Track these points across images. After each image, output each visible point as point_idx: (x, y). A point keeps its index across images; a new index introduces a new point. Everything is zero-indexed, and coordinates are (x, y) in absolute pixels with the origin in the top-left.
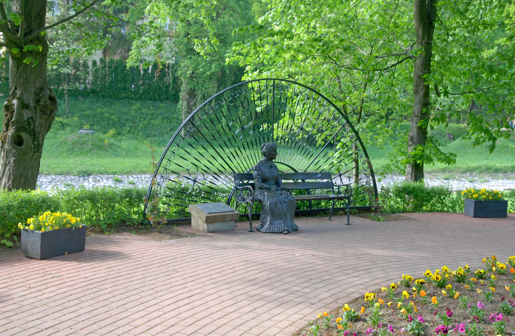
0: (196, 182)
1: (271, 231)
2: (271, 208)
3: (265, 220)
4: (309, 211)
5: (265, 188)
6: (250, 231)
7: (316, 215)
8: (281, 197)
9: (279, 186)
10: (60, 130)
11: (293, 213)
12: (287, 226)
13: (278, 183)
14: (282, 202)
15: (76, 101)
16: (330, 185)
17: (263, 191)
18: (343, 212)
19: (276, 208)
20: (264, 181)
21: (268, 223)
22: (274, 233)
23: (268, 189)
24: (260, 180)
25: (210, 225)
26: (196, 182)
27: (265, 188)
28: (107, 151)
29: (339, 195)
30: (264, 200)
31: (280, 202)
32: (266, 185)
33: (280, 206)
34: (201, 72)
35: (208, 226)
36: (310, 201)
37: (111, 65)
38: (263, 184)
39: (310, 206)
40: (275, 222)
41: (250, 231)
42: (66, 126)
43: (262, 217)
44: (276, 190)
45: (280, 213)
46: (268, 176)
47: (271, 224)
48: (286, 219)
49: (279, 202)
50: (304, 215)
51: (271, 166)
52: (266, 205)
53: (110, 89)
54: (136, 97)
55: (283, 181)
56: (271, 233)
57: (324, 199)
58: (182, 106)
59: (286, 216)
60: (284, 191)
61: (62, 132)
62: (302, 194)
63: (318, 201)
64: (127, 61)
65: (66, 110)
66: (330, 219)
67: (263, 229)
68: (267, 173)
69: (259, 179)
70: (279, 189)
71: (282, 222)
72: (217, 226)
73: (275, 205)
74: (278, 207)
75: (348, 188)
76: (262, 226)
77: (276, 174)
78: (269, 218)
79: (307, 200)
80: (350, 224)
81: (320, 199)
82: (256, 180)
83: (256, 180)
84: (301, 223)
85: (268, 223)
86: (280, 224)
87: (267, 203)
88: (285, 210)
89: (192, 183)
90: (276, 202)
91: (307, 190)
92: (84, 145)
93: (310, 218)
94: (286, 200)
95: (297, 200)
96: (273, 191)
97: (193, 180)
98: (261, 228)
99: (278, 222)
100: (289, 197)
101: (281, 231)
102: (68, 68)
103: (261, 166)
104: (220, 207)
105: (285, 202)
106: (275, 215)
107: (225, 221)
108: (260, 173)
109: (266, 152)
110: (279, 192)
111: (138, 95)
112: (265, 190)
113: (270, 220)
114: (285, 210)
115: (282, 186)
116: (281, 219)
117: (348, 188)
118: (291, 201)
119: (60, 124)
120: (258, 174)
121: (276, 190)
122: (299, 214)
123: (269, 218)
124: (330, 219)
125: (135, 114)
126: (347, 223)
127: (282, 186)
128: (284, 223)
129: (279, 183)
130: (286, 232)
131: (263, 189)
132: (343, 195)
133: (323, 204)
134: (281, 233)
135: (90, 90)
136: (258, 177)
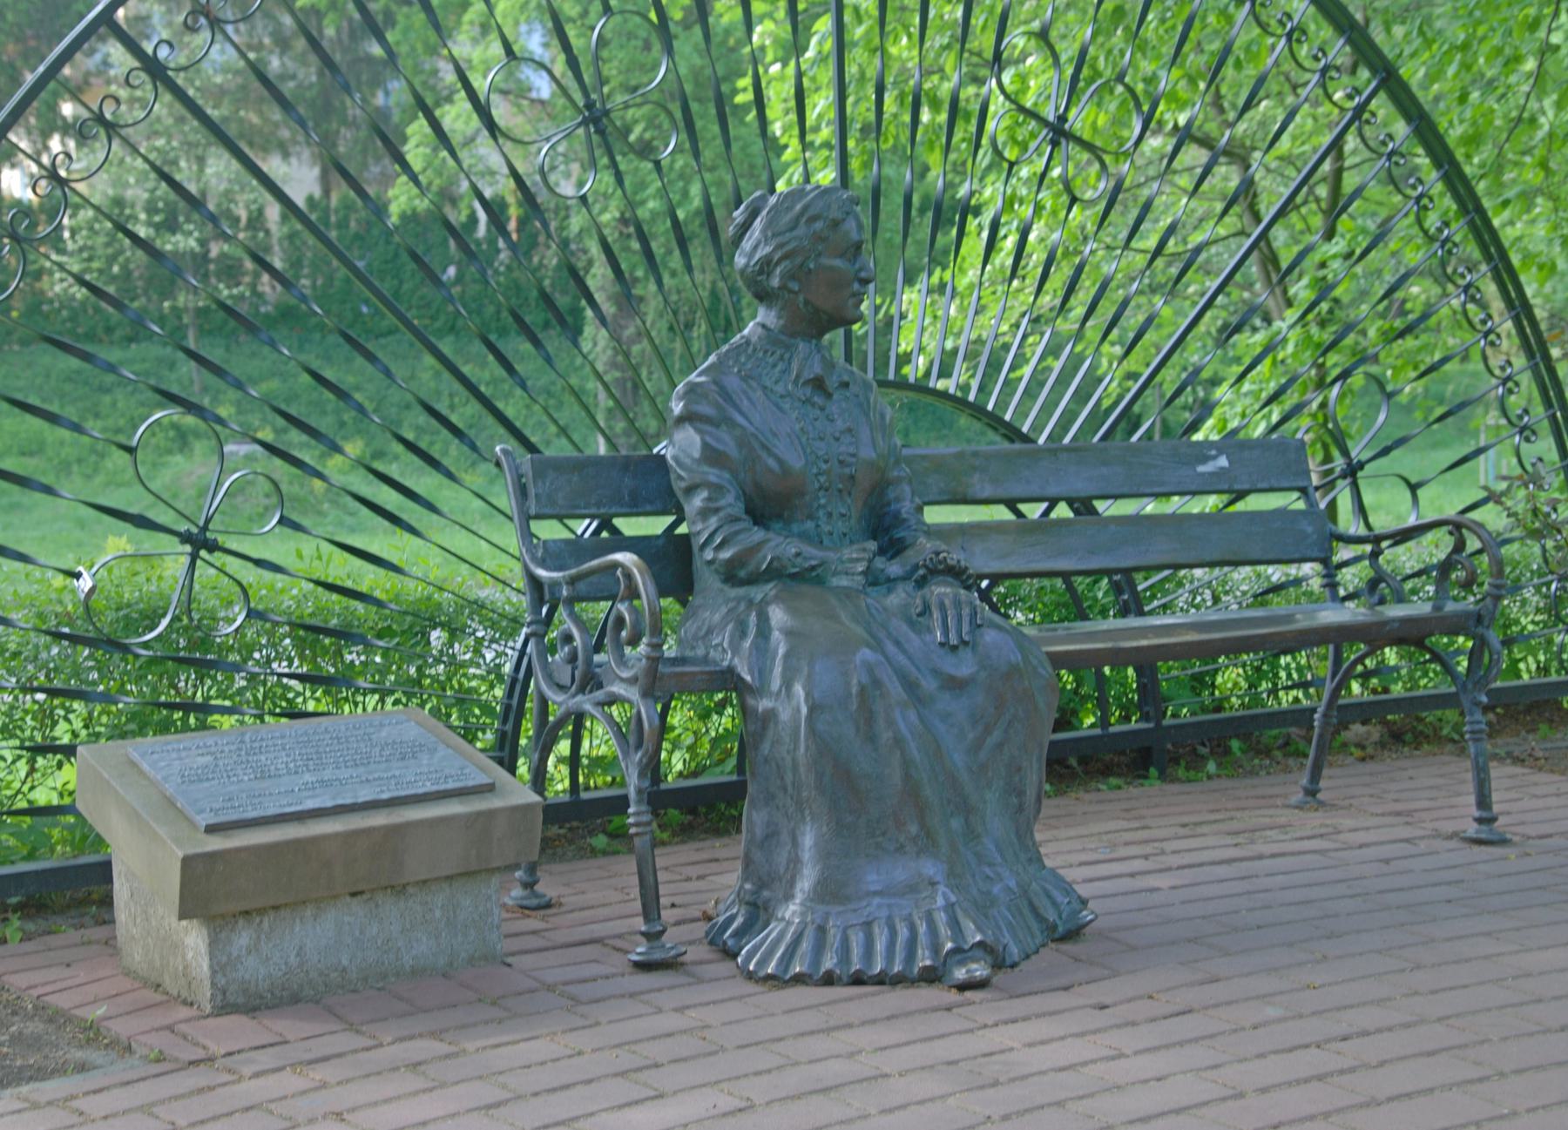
0: (213, 547)
1: (829, 962)
2: (824, 747)
3: (782, 858)
4: (1148, 737)
5: (774, 573)
6: (644, 966)
7: (1196, 762)
8: (914, 641)
9: (893, 548)
10: (170, 452)
11: (1034, 772)
12: (983, 908)
13: (885, 530)
14: (929, 684)
15: (228, 349)
16: (1317, 539)
17: (757, 593)
18: (1375, 732)
19: (872, 739)
20: (767, 506)
21: (805, 883)
22: (858, 980)
23: (798, 579)
24: (731, 502)
25: (243, 938)
26: (213, 547)
27: (774, 573)
28: (320, 513)
29: (1395, 611)
30: (763, 673)
31: (910, 686)
32: (778, 546)
33: (906, 721)
34: (651, 211)
35: (213, 944)
36: (1146, 662)
37: (346, 219)
38: (758, 534)
39: (1150, 697)
40: (873, 879)
41: (644, 966)
42: (191, 438)
43: (754, 817)
44: (874, 579)
45: (911, 790)
46: (796, 462)
47: (829, 892)
48: (971, 835)
49: (895, 689)
50: (1107, 771)
51: (818, 384)
52: (785, 715)
53: (344, 302)
54: (438, 324)
55: (935, 515)
56: (829, 980)
57: (1234, 648)
58: (595, 344)
59: (965, 808)
60: (941, 590)
61: (178, 459)
62: (1084, 617)
63: (1198, 667)
64: (391, 193)
65: (192, 382)
66: (1311, 792)
67: (765, 948)
68: (789, 440)
69: (717, 490)
70: (894, 568)
71: (930, 868)
72: (316, 938)
73: (866, 718)
74: (886, 736)
75: (1459, 546)
76: (758, 913)
77: (867, 453)
78: (808, 840)
79: (1119, 658)
80: (1503, 842)
81: (1209, 652)
82: (697, 501)
83: (697, 501)
84: (1098, 849)
85: (805, 883)
86: (917, 898)
87: (790, 704)
88: (958, 758)
89: (175, 562)
90: (872, 688)
91: (1122, 581)
92: (240, 499)
93: (1153, 788)
94: (964, 666)
95: (1058, 660)
96: (846, 593)
97: (185, 538)
98: (743, 932)
99: (900, 871)
100: (989, 636)
101: (924, 960)
102: (190, 233)
103: (733, 383)
104: (389, 754)
105: (954, 685)
106: (867, 807)
107: (399, 890)
108: (726, 441)
109: (766, 265)
110: (896, 598)
111: (442, 318)
112: (769, 589)
113: (824, 855)
114: (958, 758)
115: (925, 548)
116: (926, 843)
117: (1459, 546)
118: (1013, 672)
119: (172, 434)
120: (712, 456)
121: (874, 579)
122: (1077, 765)
123: (808, 840)
124: (1311, 792)
125: (432, 384)
126: (1472, 829)
127: (925, 548)
128: (954, 877)
129: (898, 521)
130: (979, 970)
131: (753, 580)
132: (1419, 607)
133: (1230, 677)
134: (931, 977)
135: (276, 307)
136: (713, 474)
